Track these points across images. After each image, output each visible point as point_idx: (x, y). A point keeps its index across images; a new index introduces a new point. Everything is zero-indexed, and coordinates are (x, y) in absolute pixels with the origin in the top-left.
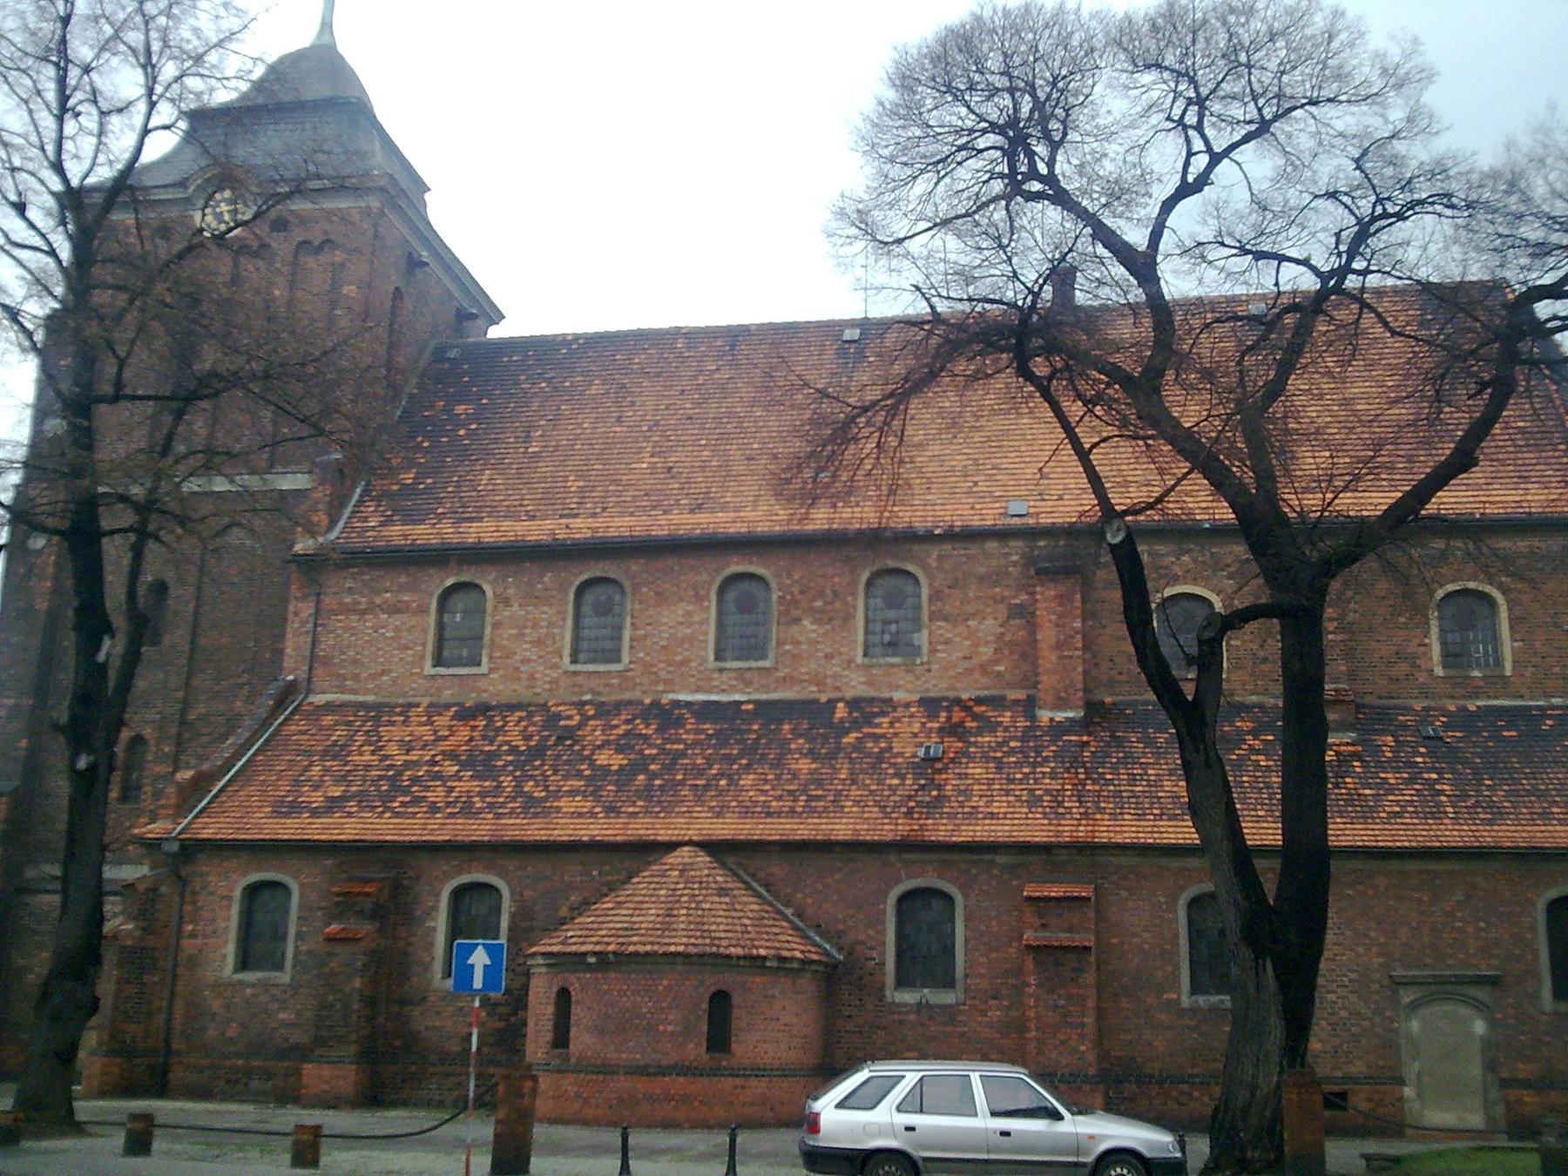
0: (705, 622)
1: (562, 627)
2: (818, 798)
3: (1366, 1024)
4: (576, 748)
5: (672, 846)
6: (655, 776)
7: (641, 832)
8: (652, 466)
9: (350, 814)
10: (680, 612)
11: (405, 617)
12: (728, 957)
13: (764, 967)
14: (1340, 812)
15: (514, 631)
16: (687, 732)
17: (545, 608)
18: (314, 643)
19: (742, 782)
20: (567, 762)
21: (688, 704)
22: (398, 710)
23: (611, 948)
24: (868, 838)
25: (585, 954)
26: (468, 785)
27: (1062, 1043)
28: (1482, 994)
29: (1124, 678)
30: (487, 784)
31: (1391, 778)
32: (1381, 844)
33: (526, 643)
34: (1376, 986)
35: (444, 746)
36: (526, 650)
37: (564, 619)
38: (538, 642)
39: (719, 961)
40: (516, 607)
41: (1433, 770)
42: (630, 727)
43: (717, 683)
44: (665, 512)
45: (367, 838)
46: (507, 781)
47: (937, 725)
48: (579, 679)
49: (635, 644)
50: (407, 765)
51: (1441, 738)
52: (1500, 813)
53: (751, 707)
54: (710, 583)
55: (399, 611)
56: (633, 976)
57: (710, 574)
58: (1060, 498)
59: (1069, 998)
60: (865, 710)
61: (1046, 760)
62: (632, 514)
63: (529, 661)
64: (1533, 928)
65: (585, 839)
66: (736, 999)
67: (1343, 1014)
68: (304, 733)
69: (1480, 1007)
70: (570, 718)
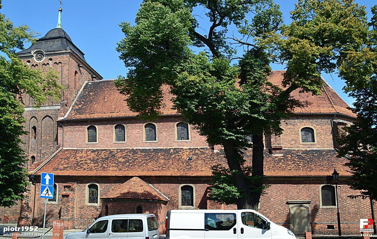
2: (164, 167)
4: (115, 158)
5: (132, 177)
6: (131, 163)
9: (68, 170)
10: (137, 131)
11: (81, 133)
12: (141, 199)
14: (278, 169)
16: (138, 155)
18: (63, 138)
19: (148, 164)
20: (113, 161)
21: (139, 149)
22: (80, 151)
23: (115, 197)
24: (174, 175)
25: (110, 198)
31: (289, 163)
32: (286, 175)
34: (284, 204)
35: (88, 157)
38: (108, 137)
41: (299, 161)
43: (145, 145)
45: (70, 175)
46: (100, 164)
47: (192, 153)
48: (117, 144)
50: (80, 161)
51: (301, 155)
52: (313, 169)
55: (79, 131)
56: (120, 203)
60: (177, 151)
61: (215, 160)
62: (125, 112)
64: (319, 192)
65: (114, 175)
67: (277, 209)
68: (61, 155)
70: (115, 152)
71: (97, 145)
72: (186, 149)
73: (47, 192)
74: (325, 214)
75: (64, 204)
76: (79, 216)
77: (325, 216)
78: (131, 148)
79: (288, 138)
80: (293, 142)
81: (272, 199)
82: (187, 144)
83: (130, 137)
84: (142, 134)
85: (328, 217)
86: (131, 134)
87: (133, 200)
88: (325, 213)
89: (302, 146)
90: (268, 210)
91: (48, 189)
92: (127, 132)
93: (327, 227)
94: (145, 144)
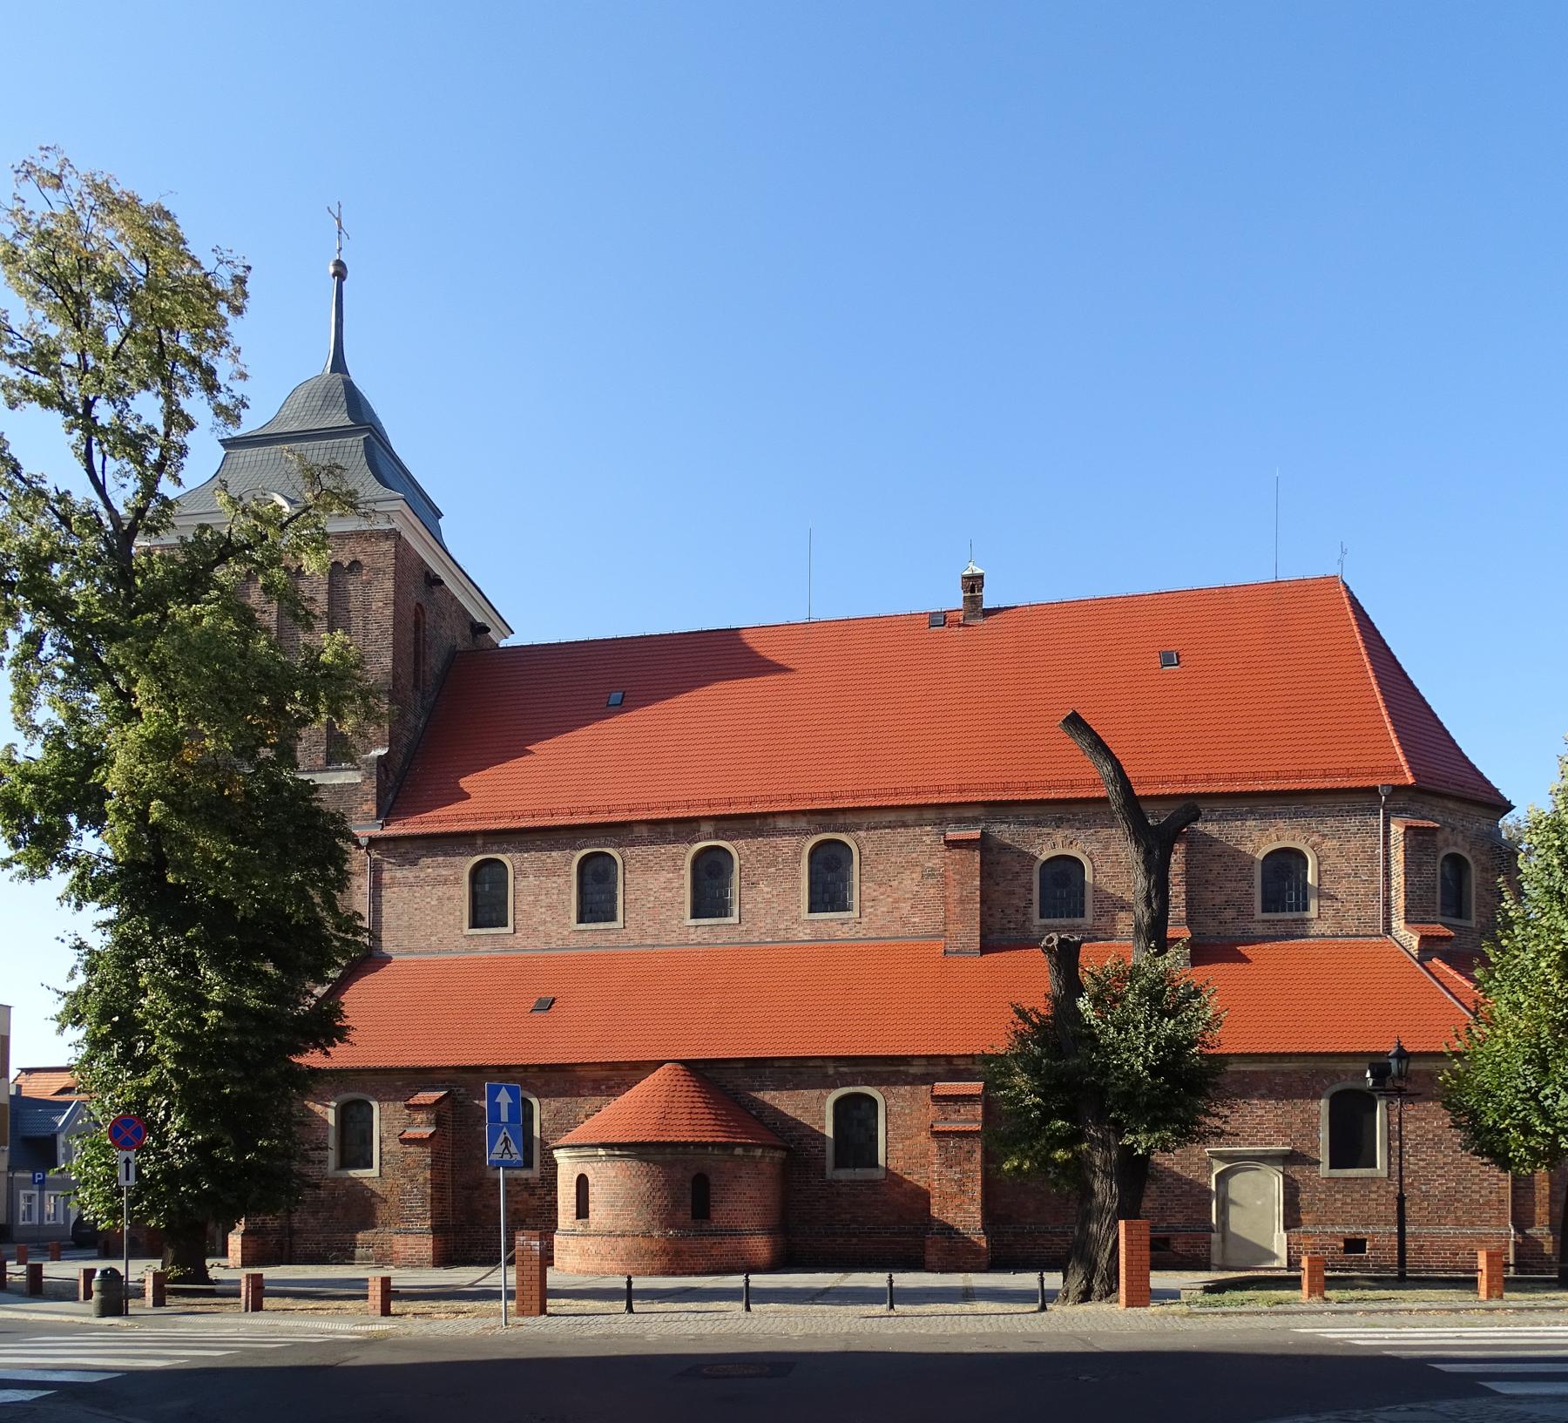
10: (662, 880)
29: (1012, 925)
38: (550, 907)
40: (531, 878)
48: (586, 935)
59: (963, 1172)
66: (713, 1179)
67: (1169, 1180)
73: (506, 1147)
84: (682, 892)
91: (508, 1135)
93: (1342, 1245)
94: (692, 930)
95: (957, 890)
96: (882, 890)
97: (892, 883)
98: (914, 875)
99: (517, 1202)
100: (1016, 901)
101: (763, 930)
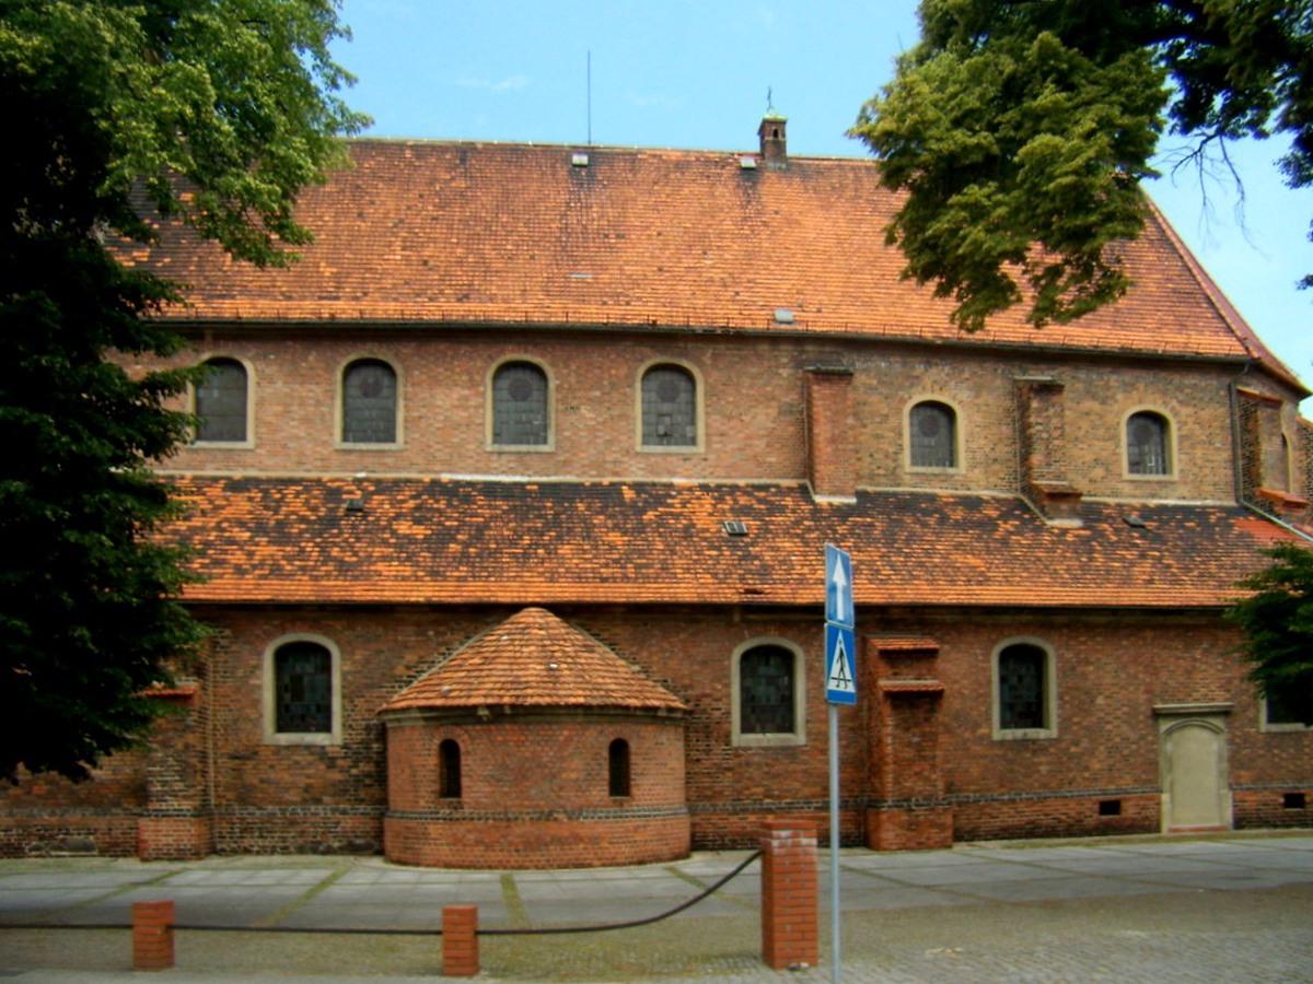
0: (482, 406)
1: (332, 406)
2: (647, 566)
3: (1134, 747)
5: (515, 608)
7: (479, 594)
8: (407, 259)
10: (455, 396)
12: (627, 708)
13: (655, 717)
15: (279, 409)
17: (313, 387)
25: (475, 707)
26: (265, 550)
27: (917, 774)
28: (1218, 722)
29: (882, 472)
30: (288, 549)
33: (293, 420)
34: (1141, 717)
36: (293, 427)
37: (332, 398)
38: (306, 420)
39: (619, 712)
40: (280, 384)
42: (418, 501)
44: (431, 300)
48: (353, 457)
49: (409, 425)
53: (535, 487)
54: (484, 369)
57: (485, 364)
58: (819, 311)
59: (923, 735)
63: (298, 438)
65: (421, 599)
66: (633, 746)
67: (1117, 740)
69: (1216, 731)
71: (249, 459)
72: (690, 489)
74: (1274, 755)
75: (160, 737)
76: (230, 795)
77: (1277, 760)
78: (427, 478)
79: (1081, 453)
80: (1099, 472)
81: (1100, 701)
82: (688, 465)
83: (423, 424)
84: (481, 411)
85: (1284, 764)
86: (424, 411)
87: (596, 711)
88: (1276, 751)
89: (1127, 488)
90: (1085, 743)
92: (406, 399)
93: (1282, 800)
95: (828, 427)
96: (732, 424)
97: (744, 417)
98: (770, 411)
99: (308, 777)
100: (885, 446)
101: (586, 462)
